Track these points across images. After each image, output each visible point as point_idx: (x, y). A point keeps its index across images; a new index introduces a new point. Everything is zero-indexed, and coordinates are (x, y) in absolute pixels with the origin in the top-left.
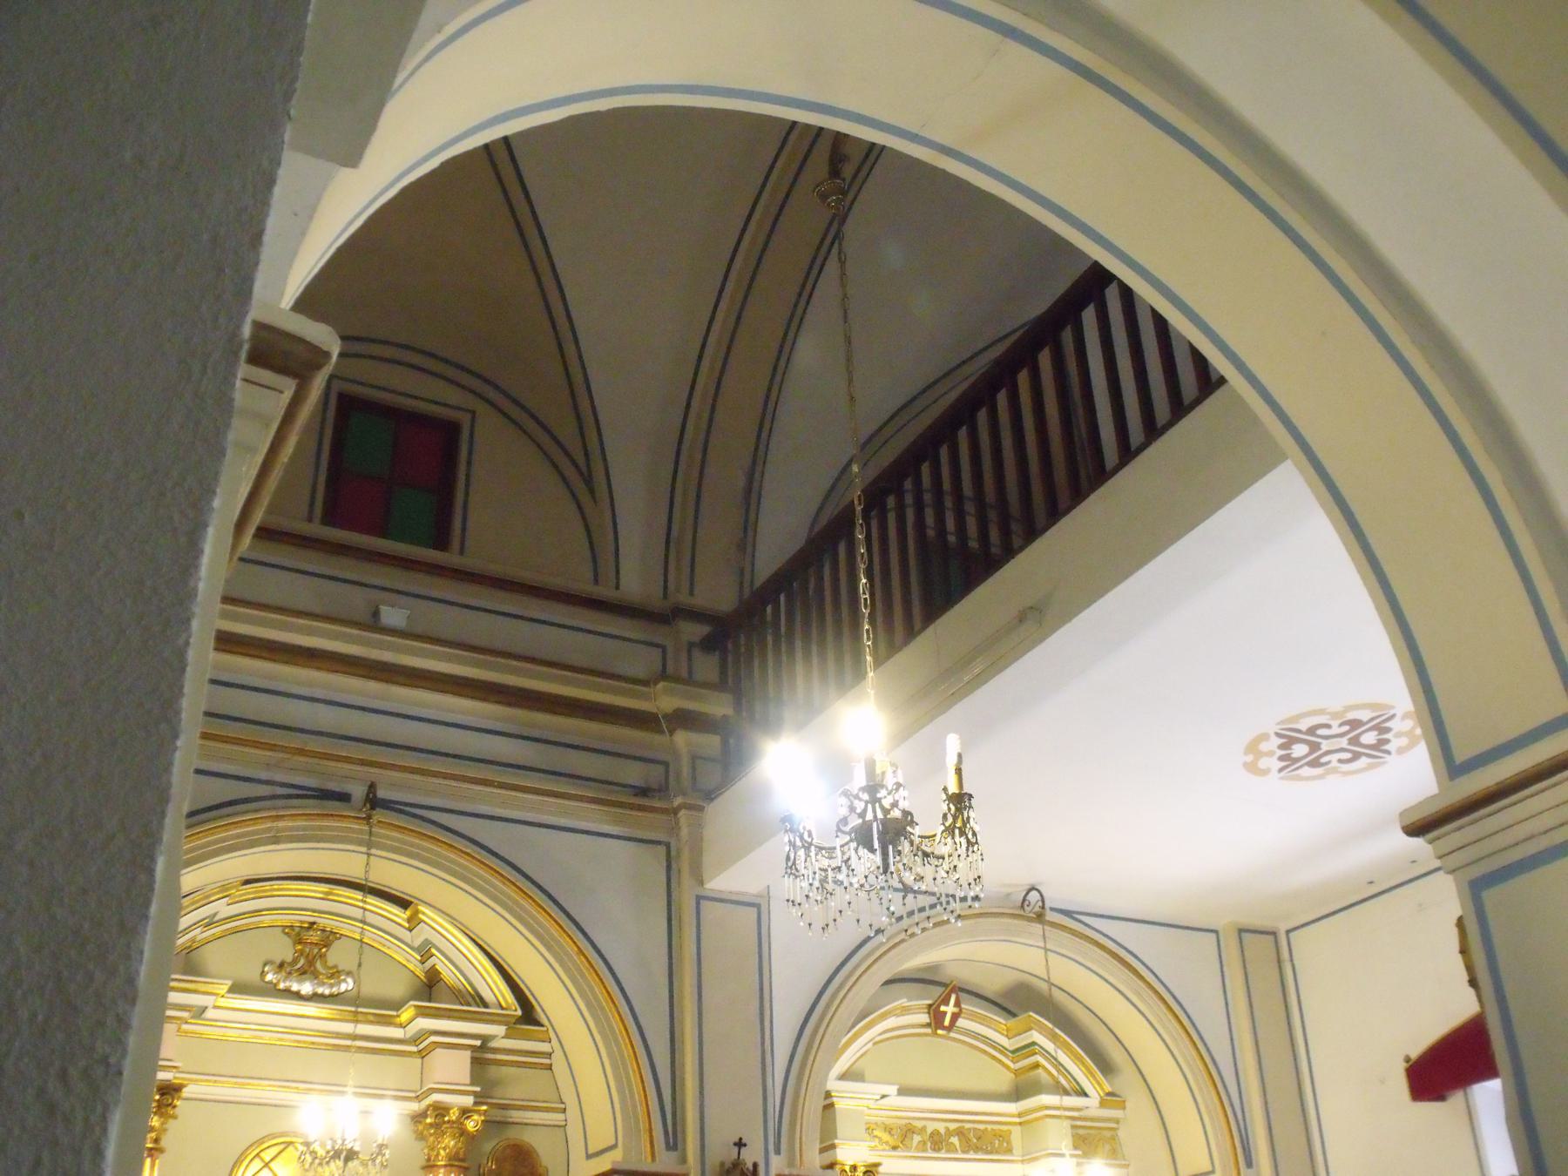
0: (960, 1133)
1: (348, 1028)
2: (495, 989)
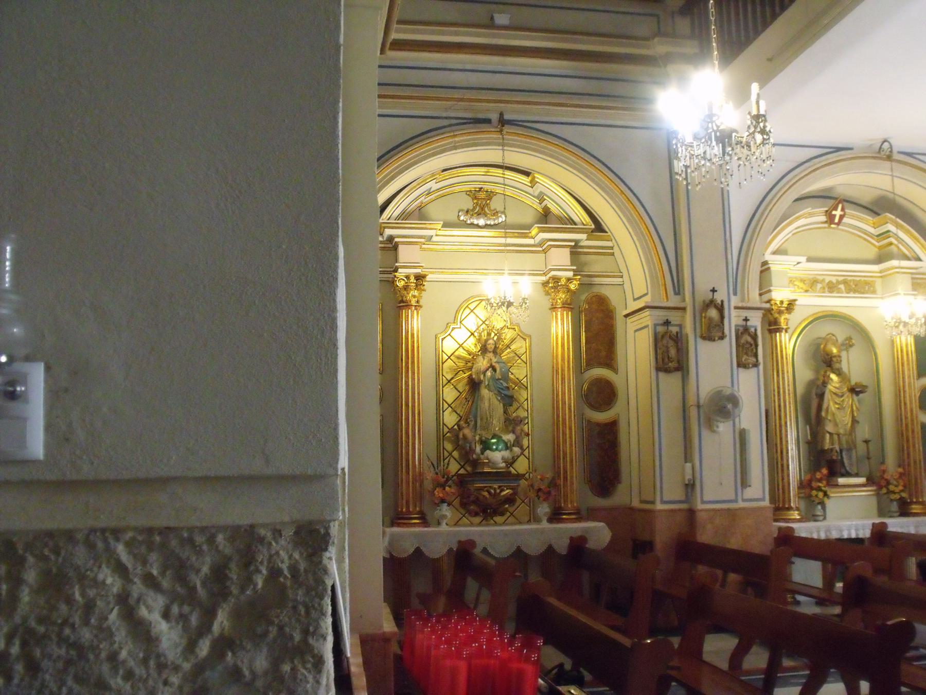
0: (845, 282)
1: (502, 241)
2: (579, 215)
